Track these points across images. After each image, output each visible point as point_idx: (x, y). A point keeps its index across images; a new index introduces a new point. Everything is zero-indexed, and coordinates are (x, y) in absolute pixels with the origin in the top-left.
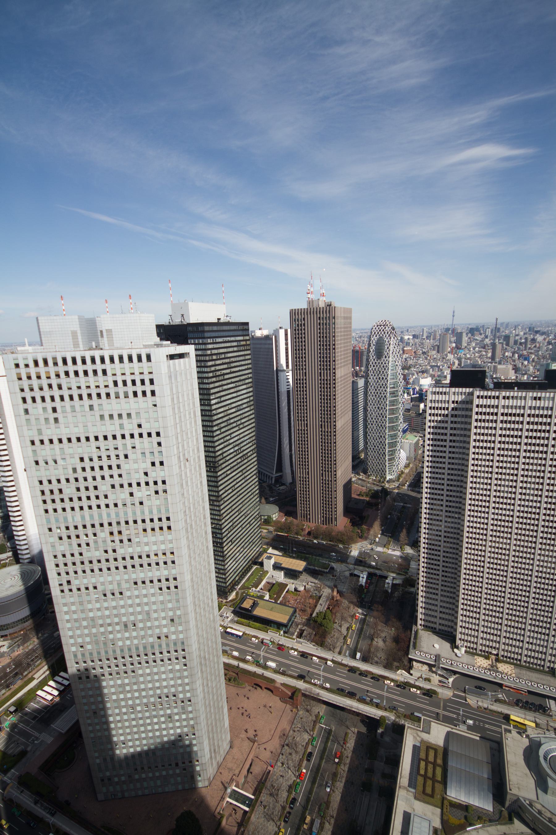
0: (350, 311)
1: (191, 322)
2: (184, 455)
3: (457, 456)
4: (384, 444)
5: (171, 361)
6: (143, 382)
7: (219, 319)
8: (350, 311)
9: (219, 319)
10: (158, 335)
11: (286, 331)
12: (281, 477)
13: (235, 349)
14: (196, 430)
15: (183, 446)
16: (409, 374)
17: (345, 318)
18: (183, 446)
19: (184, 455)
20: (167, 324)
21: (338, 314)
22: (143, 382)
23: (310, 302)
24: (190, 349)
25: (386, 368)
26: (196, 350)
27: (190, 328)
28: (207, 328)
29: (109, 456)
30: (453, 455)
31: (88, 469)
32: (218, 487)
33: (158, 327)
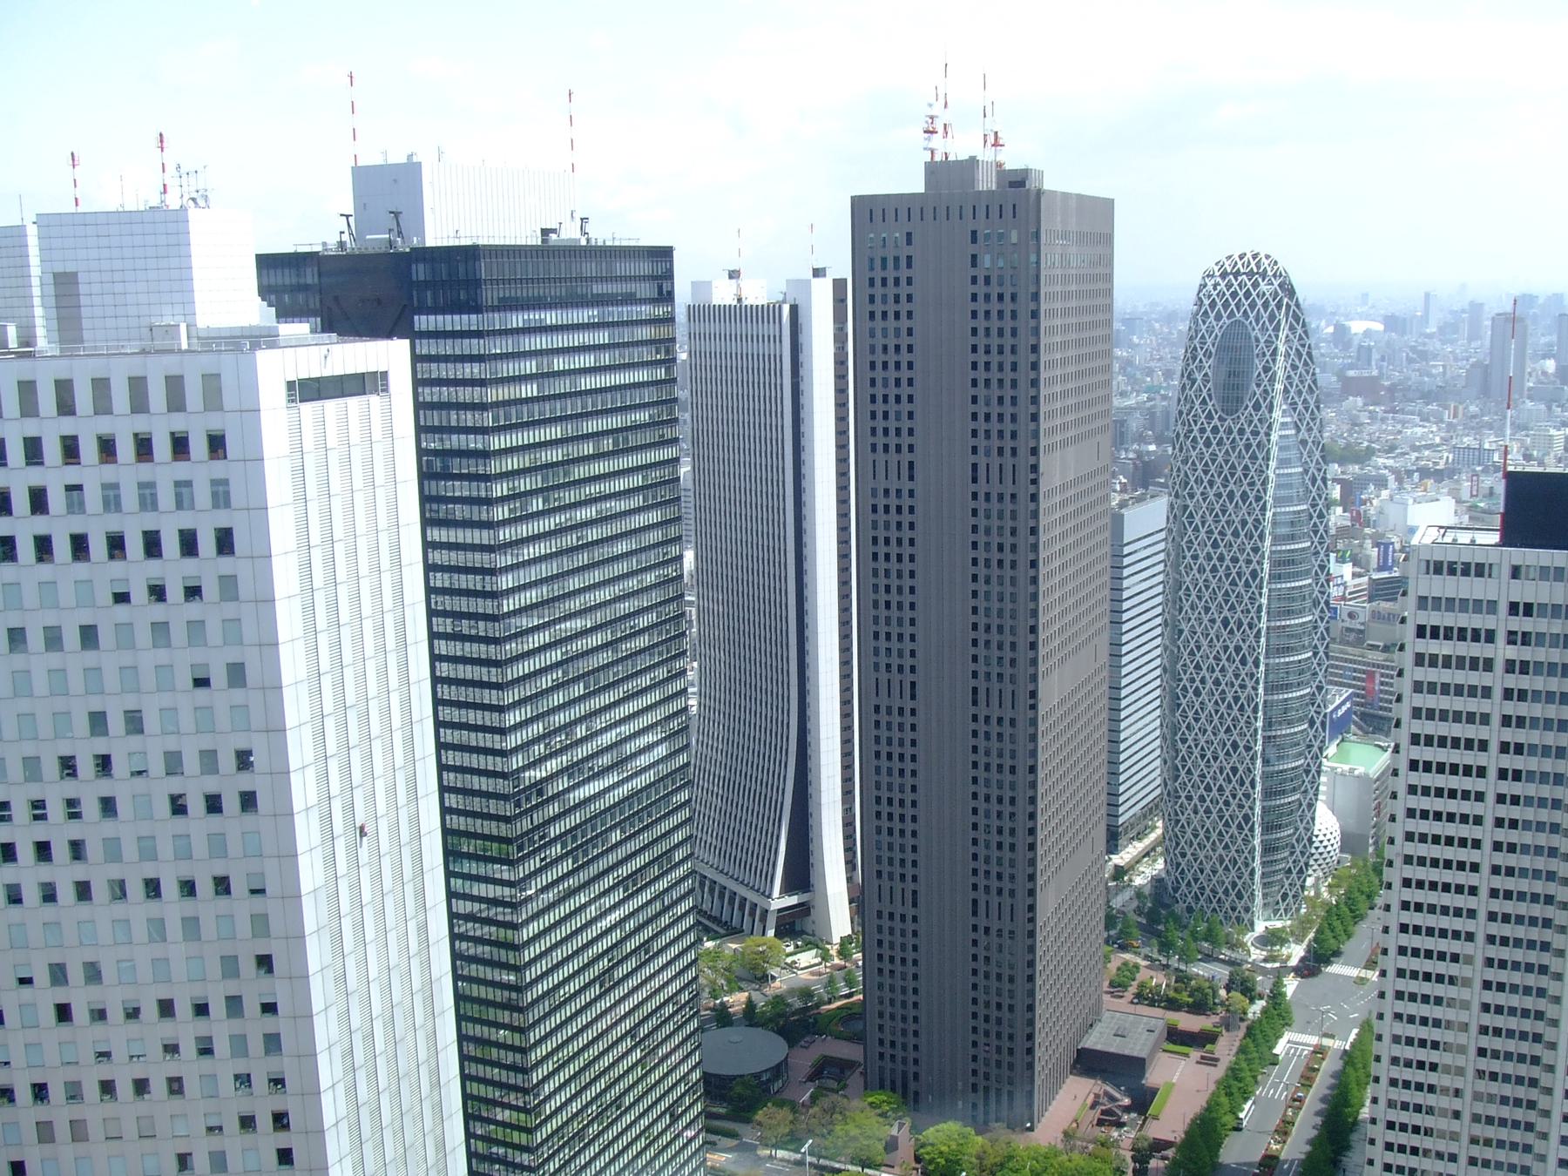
0: (1105, 208)
1: (430, 242)
2: (350, 808)
3: (1528, 838)
4: (1246, 781)
5: (308, 408)
6: (886, 448)
7: (545, 232)
8: (1105, 208)
9: (545, 232)
10: (265, 291)
11: (839, 285)
12: (804, 910)
13: (606, 359)
14: (407, 703)
15: (347, 769)
16: (1363, 482)
17: (1083, 238)
18: (347, 769)
19: (350, 808)
20: (332, 248)
21: (1050, 223)
22: (886, 448)
23: (935, 171)
24: (391, 356)
25: (1258, 452)
26: (416, 359)
27: (265, 282)
28: (590, 268)
29: (38, 804)
30: (1514, 836)
31: (908, 803)
32: (516, 948)
33: (266, 263)
